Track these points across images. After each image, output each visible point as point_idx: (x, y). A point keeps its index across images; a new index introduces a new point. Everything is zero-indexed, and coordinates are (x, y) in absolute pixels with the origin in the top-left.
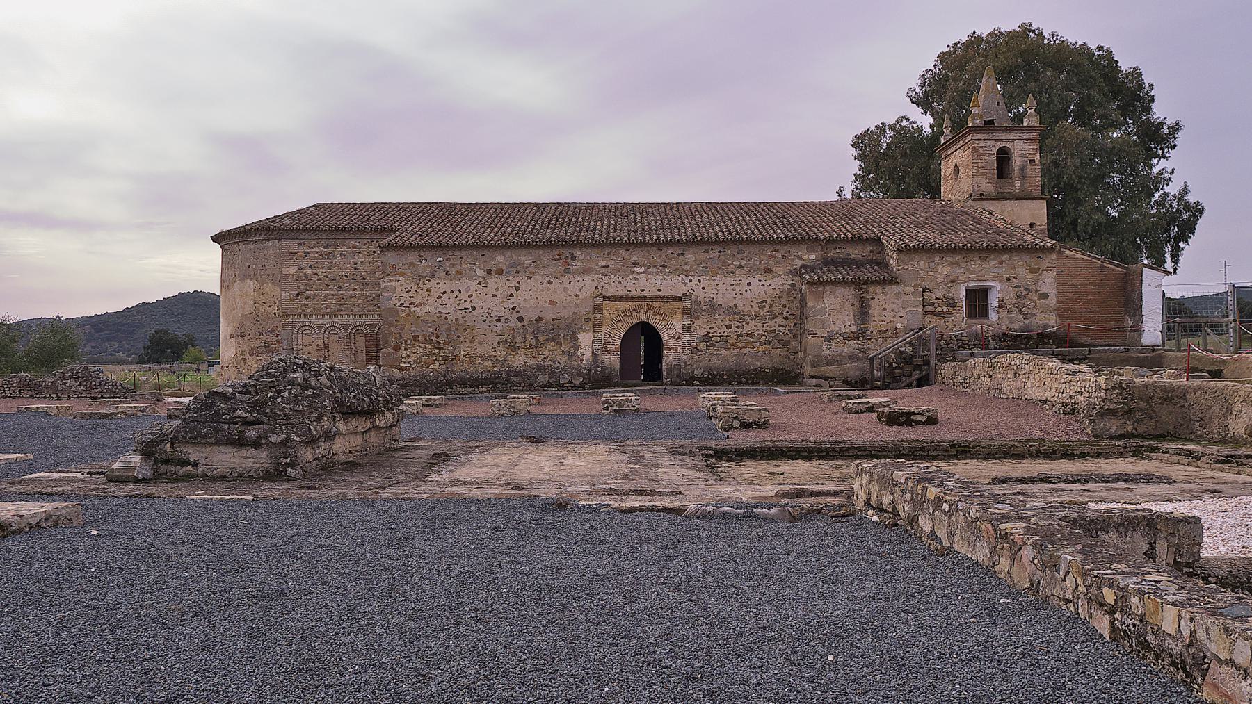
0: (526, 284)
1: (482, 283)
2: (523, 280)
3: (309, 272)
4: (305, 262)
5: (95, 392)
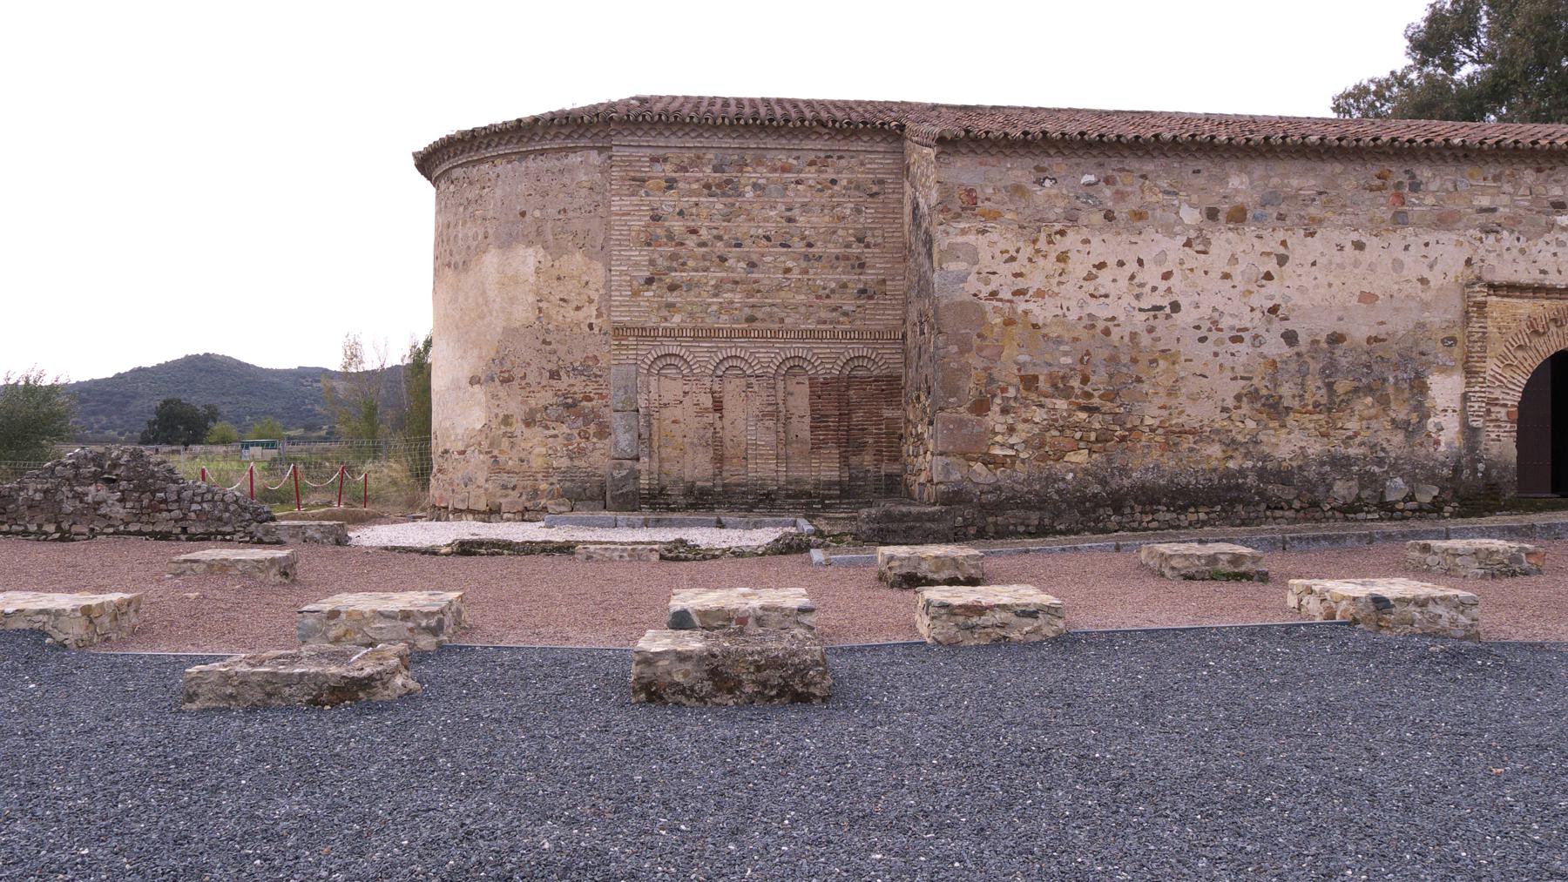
0: (1303, 248)
1: (1198, 243)
2: (1296, 239)
3: (678, 226)
4: (668, 202)
5: (164, 521)
